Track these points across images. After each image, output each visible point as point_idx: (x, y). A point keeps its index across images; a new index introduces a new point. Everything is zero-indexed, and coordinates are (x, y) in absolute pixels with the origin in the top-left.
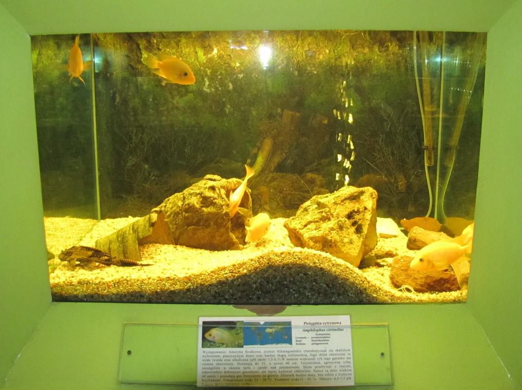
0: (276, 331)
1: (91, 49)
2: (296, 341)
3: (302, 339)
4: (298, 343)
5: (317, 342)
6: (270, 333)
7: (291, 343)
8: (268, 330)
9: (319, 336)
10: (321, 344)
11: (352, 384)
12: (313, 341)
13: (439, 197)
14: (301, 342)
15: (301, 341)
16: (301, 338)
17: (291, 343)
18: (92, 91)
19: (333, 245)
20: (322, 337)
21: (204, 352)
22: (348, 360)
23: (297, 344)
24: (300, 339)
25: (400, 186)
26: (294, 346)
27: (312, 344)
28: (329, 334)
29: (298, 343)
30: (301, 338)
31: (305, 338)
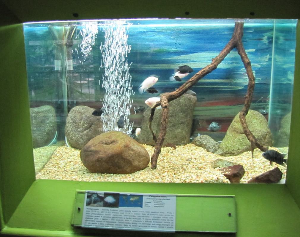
0: (135, 200)
1: (275, 27)
2: (145, 204)
3: (149, 203)
4: (146, 205)
5: (157, 206)
6: (132, 201)
7: (142, 207)
8: (131, 199)
9: (162, 206)
10: (161, 207)
11: (173, 230)
12: (155, 205)
13: (27, 24)
14: (148, 205)
15: (148, 204)
16: (148, 202)
17: (142, 207)
18: (226, 86)
19: (238, 175)
20: (160, 203)
21: (87, 209)
22: (172, 217)
23: (145, 206)
24: (147, 203)
25: (84, 47)
26: (144, 209)
27: (155, 206)
28: (164, 205)
29: (146, 205)
30: (148, 202)
31: (150, 203)
